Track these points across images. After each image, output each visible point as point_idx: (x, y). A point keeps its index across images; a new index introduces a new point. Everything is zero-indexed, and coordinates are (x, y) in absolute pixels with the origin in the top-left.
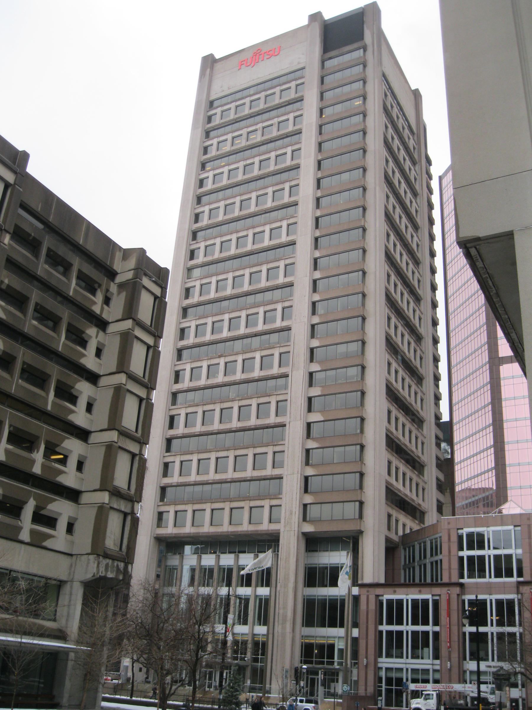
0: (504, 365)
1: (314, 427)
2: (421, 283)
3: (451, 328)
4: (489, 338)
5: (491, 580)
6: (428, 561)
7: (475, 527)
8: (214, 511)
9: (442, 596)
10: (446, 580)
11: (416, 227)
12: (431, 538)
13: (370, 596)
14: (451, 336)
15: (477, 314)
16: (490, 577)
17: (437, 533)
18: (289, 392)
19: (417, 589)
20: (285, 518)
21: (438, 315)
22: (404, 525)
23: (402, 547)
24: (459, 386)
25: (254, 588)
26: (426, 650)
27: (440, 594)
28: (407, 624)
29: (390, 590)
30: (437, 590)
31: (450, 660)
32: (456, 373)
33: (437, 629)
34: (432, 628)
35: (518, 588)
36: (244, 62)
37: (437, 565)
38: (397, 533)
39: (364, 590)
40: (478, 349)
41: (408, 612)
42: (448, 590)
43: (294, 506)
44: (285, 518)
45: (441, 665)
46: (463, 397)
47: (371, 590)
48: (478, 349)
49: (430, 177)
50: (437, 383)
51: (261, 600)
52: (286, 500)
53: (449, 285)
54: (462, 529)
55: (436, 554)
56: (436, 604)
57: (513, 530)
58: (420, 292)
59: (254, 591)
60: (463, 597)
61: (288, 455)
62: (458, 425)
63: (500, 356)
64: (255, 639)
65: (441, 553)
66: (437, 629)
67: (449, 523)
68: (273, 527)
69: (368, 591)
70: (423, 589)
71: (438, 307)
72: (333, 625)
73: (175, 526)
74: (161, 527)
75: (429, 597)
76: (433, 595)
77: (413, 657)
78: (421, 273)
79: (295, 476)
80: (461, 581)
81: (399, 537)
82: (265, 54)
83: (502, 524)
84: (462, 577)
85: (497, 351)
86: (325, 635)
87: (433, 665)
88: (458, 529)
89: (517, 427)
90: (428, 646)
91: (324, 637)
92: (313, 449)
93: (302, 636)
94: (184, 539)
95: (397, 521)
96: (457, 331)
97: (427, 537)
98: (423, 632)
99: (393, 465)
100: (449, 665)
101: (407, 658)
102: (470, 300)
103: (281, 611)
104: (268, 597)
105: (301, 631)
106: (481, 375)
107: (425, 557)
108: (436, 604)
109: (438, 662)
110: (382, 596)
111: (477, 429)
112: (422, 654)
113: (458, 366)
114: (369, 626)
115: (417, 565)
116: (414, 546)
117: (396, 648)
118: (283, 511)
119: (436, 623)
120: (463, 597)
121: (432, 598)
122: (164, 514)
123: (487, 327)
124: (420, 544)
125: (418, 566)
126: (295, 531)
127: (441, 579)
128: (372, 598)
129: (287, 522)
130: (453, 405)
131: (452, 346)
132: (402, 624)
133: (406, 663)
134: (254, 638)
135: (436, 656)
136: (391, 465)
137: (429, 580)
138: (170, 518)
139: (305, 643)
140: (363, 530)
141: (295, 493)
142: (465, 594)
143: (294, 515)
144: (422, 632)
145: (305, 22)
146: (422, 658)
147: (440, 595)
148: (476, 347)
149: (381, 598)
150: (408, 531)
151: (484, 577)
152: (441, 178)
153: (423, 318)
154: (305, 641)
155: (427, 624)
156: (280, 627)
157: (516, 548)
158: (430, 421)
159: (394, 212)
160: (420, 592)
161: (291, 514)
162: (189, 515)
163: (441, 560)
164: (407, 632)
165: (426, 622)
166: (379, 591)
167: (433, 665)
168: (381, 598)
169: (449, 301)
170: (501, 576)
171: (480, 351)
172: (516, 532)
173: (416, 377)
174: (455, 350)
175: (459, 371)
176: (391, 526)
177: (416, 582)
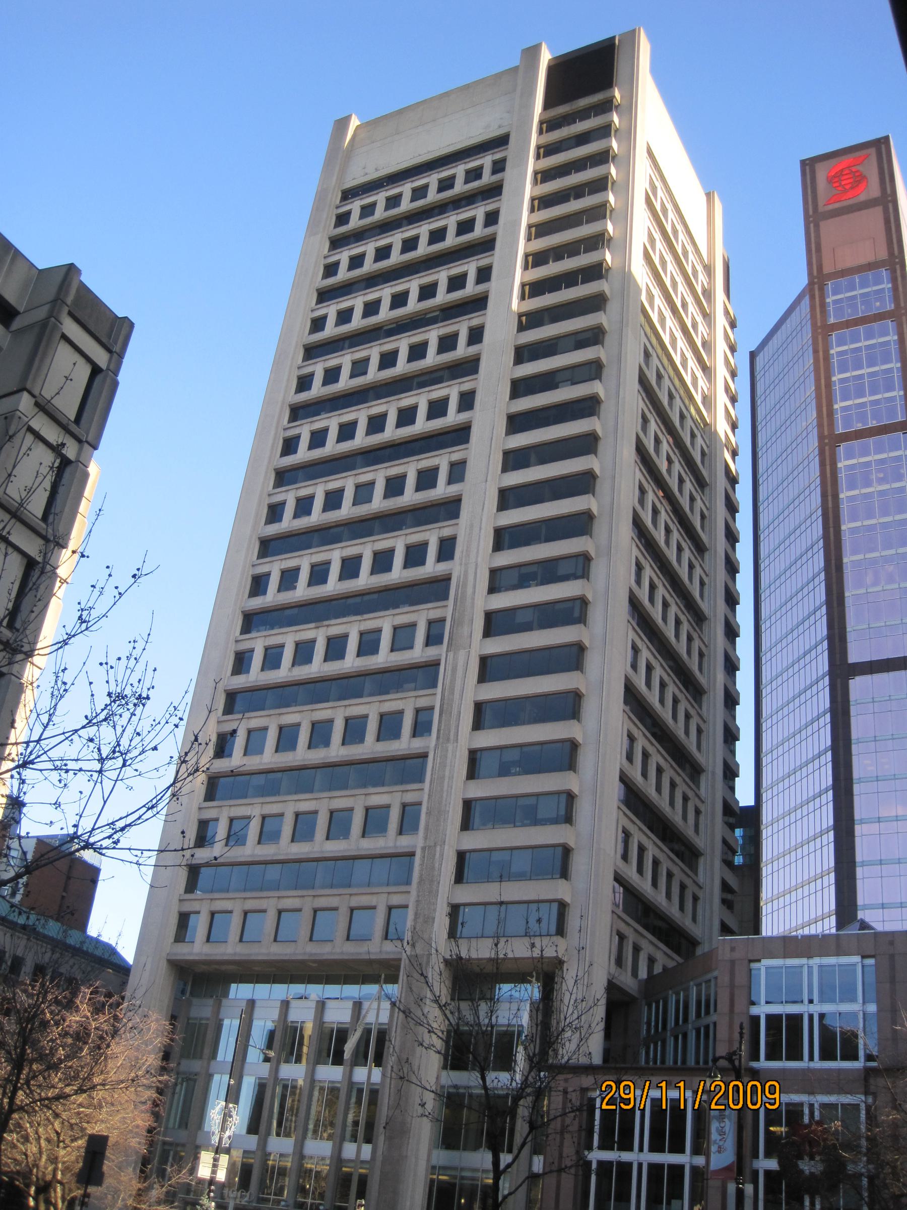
0: (857, 678)
1: (466, 914)
2: (707, 522)
3: (765, 747)
4: (830, 626)
5: (812, 1065)
6: (690, 1026)
8: (283, 914)
11: (700, 548)
14: (764, 728)
15: (811, 586)
16: (811, 1058)
21: (739, 721)
22: (651, 961)
23: (644, 1002)
25: (348, 1069)
28: (641, 1149)
32: (770, 839)
33: (700, 1161)
34: (691, 1159)
35: (866, 1080)
37: (706, 1033)
38: (635, 973)
40: (810, 651)
41: (642, 1128)
48: (810, 651)
50: (731, 783)
53: (763, 662)
54: (759, 961)
55: (708, 1012)
56: (701, 1115)
57: (860, 964)
58: (704, 606)
59: (348, 1073)
64: (344, 1169)
65: (715, 1010)
66: (700, 1161)
67: (733, 949)
73: (208, 940)
74: (184, 941)
78: (706, 640)
80: (754, 1064)
81: (640, 981)
83: (839, 953)
84: (757, 1059)
88: (751, 961)
89: (878, 792)
90: (680, 1197)
92: (465, 905)
93: (434, 1168)
94: (224, 968)
95: (637, 949)
96: (774, 686)
97: (692, 980)
98: (672, 1167)
99: (633, 842)
104: (387, 1027)
106: (815, 698)
107: (686, 1020)
108: (701, 1115)
111: (806, 919)
115: (671, 1035)
117: (615, 1200)
119: (696, 1151)
122: (192, 916)
123: (826, 575)
124: (678, 994)
125: (672, 1038)
131: (765, 783)
132: (630, 1148)
136: (631, 839)
137: (691, 1062)
138: (199, 925)
139: (439, 1181)
148: (807, 647)
150: (658, 969)
151: (800, 1058)
153: (701, 898)
154: (440, 1177)
155: (682, 1150)
157: (864, 1003)
158: (713, 773)
162: (236, 920)
163: (715, 1024)
164: (640, 1165)
165: (678, 1148)
170: (833, 1058)
171: (812, 618)
172: (865, 969)
173: (687, 766)
174: (769, 687)
176: (624, 959)
177: (667, 1063)
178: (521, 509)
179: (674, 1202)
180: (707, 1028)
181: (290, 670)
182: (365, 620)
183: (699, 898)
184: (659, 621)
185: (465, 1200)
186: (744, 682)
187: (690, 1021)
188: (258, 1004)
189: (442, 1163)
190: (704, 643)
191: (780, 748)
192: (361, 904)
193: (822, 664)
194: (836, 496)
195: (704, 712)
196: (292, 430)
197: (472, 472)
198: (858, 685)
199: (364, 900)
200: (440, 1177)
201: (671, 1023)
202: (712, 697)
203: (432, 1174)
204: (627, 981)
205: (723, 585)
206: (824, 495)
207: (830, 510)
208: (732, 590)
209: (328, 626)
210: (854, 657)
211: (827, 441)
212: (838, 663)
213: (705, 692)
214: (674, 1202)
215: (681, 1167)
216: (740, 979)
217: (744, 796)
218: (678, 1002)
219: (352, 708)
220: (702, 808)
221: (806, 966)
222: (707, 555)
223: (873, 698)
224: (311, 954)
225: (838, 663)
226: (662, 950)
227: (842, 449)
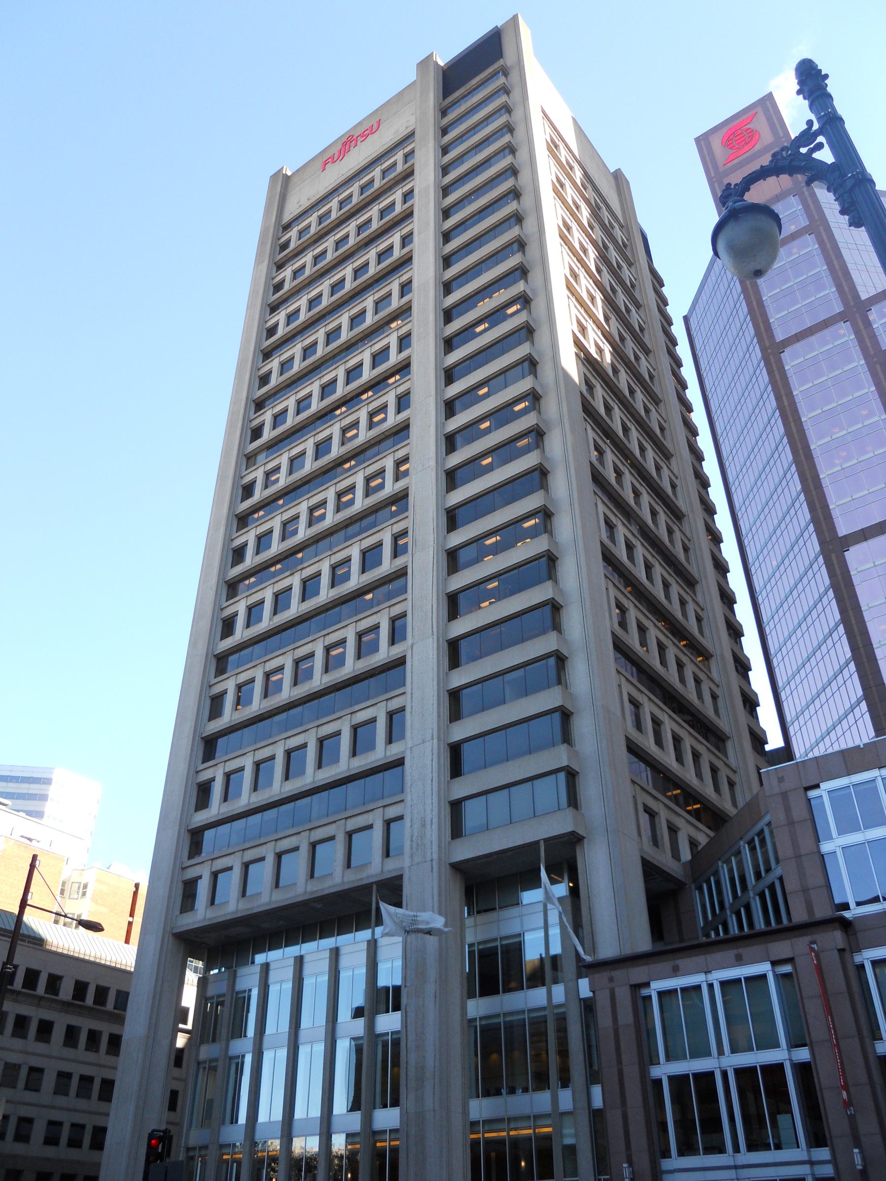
6: (751, 894)
7: (849, 774)
9: (798, 961)
10: (799, 915)
11: (690, 582)
12: (748, 837)
13: (617, 991)
17: (761, 818)
18: (410, 598)
19: (729, 954)
20: (412, 836)
21: (747, 651)
23: (693, 886)
24: (802, 722)
26: (782, 1119)
27: (790, 955)
29: (665, 966)
30: (782, 948)
31: (857, 1143)
34: (789, 1054)
36: (330, 160)
38: (676, 855)
39: (602, 977)
42: (814, 942)
43: (428, 808)
44: (412, 836)
45: (834, 1161)
46: (813, 740)
47: (618, 974)
49: (668, 321)
51: (385, 1045)
52: (412, 799)
54: (817, 786)
55: (768, 870)
58: (693, 570)
60: (858, 959)
61: (412, 707)
62: (796, 723)
63: (840, 535)
64: (378, 1144)
67: (781, 780)
68: (392, 867)
69: (611, 980)
70: (747, 951)
71: (710, 486)
72: (541, 1081)
75: (764, 968)
76: (774, 963)
77: (751, 1147)
79: (428, 745)
81: (684, 864)
82: (359, 138)
85: (832, 527)
86: (527, 1111)
87: (811, 1163)
88: (808, 789)
91: (528, 1117)
93: (474, 1124)
99: (644, 712)
100: (858, 1159)
101: (737, 1149)
102: (795, 593)
103: (413, 1058)
105: (465, 1111)
109: (823, 1153)
110: (647, 985)
112: (776, 1135)
113: (792, 683)
114: (625, 1068)
115: (732, 912)
116: (716, 873)
117: (702, 1133)
118: (407, 831)
119: (795, 1043)
120: (858, 959)
121: (774, 972)
126: (432, 860)
127: (790, 919)
128: (624, 995)
129: (415, 845)
130: (788, 725)
133: (736, 1167)
134: (376, 1142)
135: (817, 1139)
137: (760, 924)
140: (581, 832)
141: (429, 781)
142: (859, 950)
143: (429, 826)
144: (763, 1067)
145: (411, 76)
146: (778, 1147)
147: (790, 960)
149: (644, 992)
152: (686, 319)
154: (486, 1135)
156: (411, 1096)
158: (722, 656)
159: (671, 541)
160: (739, 961)
161: (423, 825)
163: (781, 879)
166: (637, 974)
167: (811, 1163)
168: (644, 992)
169: (783, 696)
175: (795, 693)
177: (732, 932)
178: (468, 411)
179: (780, 1118)
180: (772, 887)
181: (271, 619)
182: (334, 553)
183: (735, 783)
184: (678, 685)
185: (525, 1164)
186: (751, 646)
187: (750, 887)
188: (272, 966)
189: (486, 1115)
190: (699, 606)
191: (797, 677)
192: (358, 826)
193: (814, 545)
194: (790, 394)
195: (700, 598)
196: (258, 419)
197: (416, 399)
198: (854, 556)
199: (360, 821)
200: (486, 1135)
201: (728, 898)
202: (704, 585)
203: (472, 1133)
204: (664, 859)
205: (716, 583)
206: (778, 398)
207: (788, 408)
208: (719, 557)
209: (301, 570)
210: (843, 529)
211: (770, 351)
212: (828, 540)
213: (697, 582)
214: (780, 1118)
215: (780, 1067)
216: (798, 813)
217: (775, 741)
218: (731, 871)
219: (331, 635)
220: (718, 692)
221: (879, 779)
222: (698, 588)
223: (874, 562)
224: (313, 893)
225: (828, 540)
226: (704, 832)
227: (786, 356)
